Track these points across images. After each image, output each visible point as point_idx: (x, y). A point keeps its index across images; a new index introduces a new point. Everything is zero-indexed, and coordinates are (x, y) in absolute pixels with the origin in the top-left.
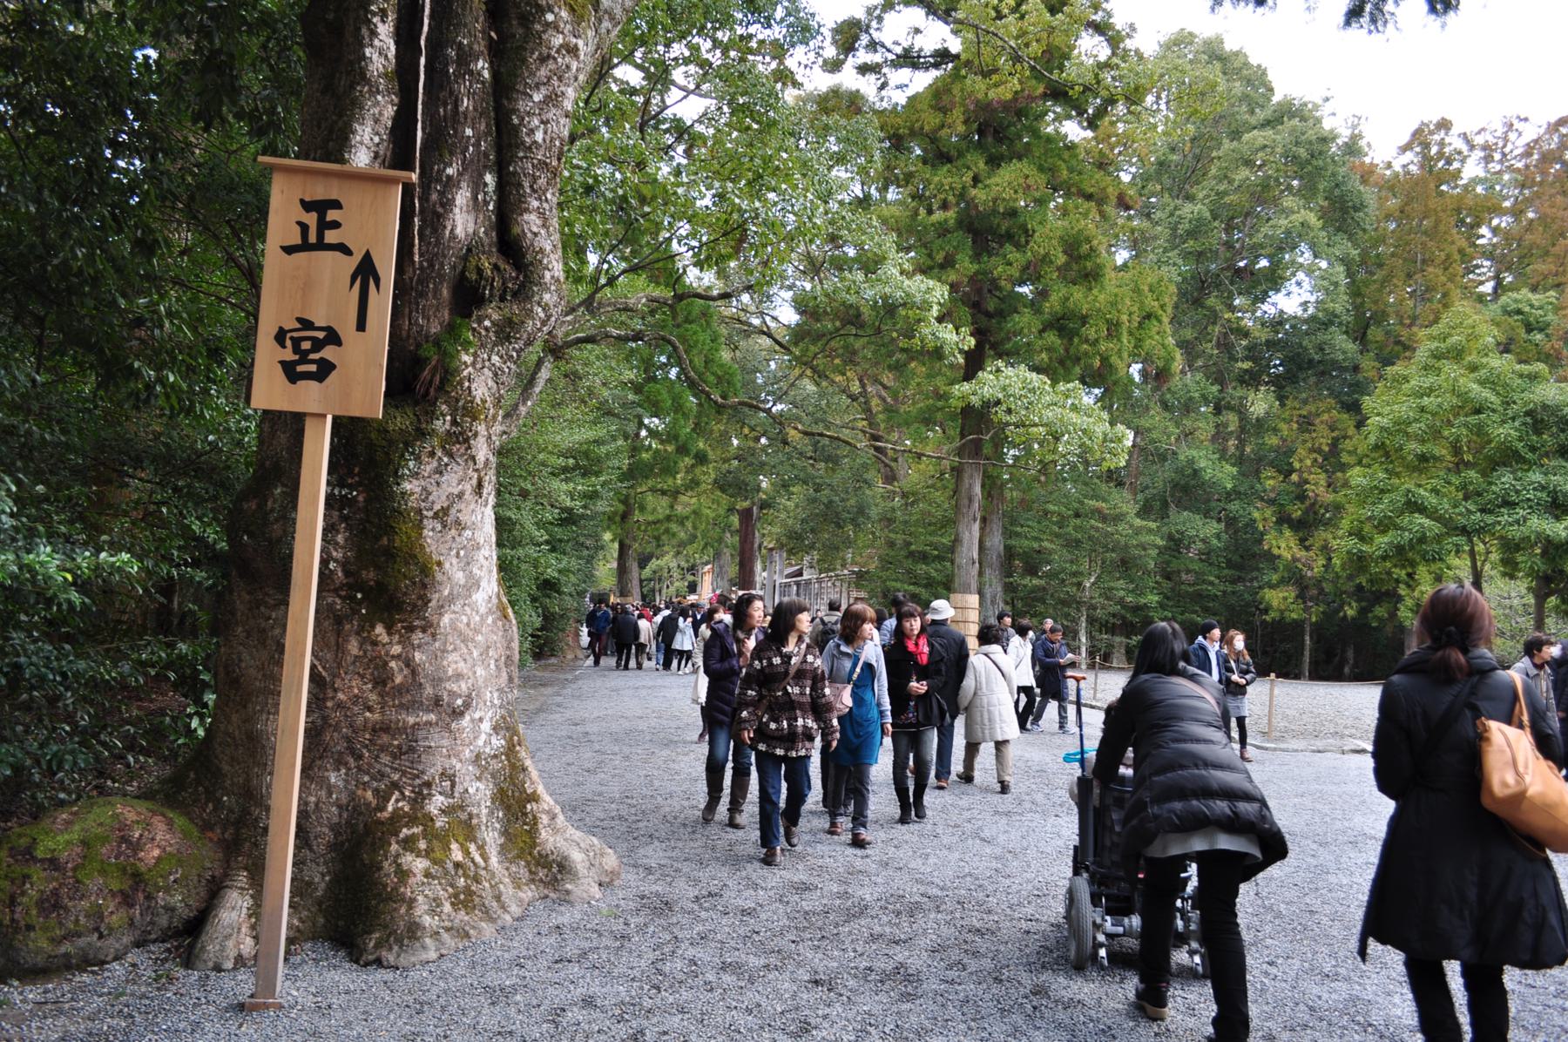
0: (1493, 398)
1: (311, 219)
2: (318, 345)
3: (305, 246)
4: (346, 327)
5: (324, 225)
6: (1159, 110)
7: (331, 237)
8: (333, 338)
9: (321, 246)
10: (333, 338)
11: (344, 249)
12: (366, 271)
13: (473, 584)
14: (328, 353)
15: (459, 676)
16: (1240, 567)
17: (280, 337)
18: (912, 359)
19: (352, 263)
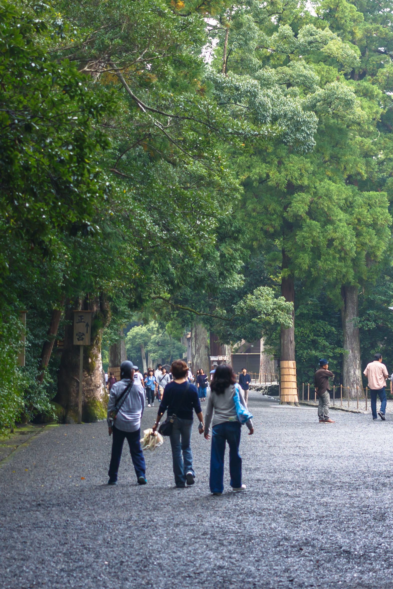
0: (351, 52)
1: (80, 318)
2: (82, 336)
3: (79, 322)
4: (85, 332)
5: (82, 319)
6: (264, 524)
7: (83, 320)
8: (83, 334)
9: (81, 322)
10: (83, 334)
11: (84, 322)
12: (87, 325)
13: (99, 367)
14: (83, 337)
15: (328, 272)
16: (351, 497)
17: (77, 335)
18: (144, 375)
19: (85, 324)
